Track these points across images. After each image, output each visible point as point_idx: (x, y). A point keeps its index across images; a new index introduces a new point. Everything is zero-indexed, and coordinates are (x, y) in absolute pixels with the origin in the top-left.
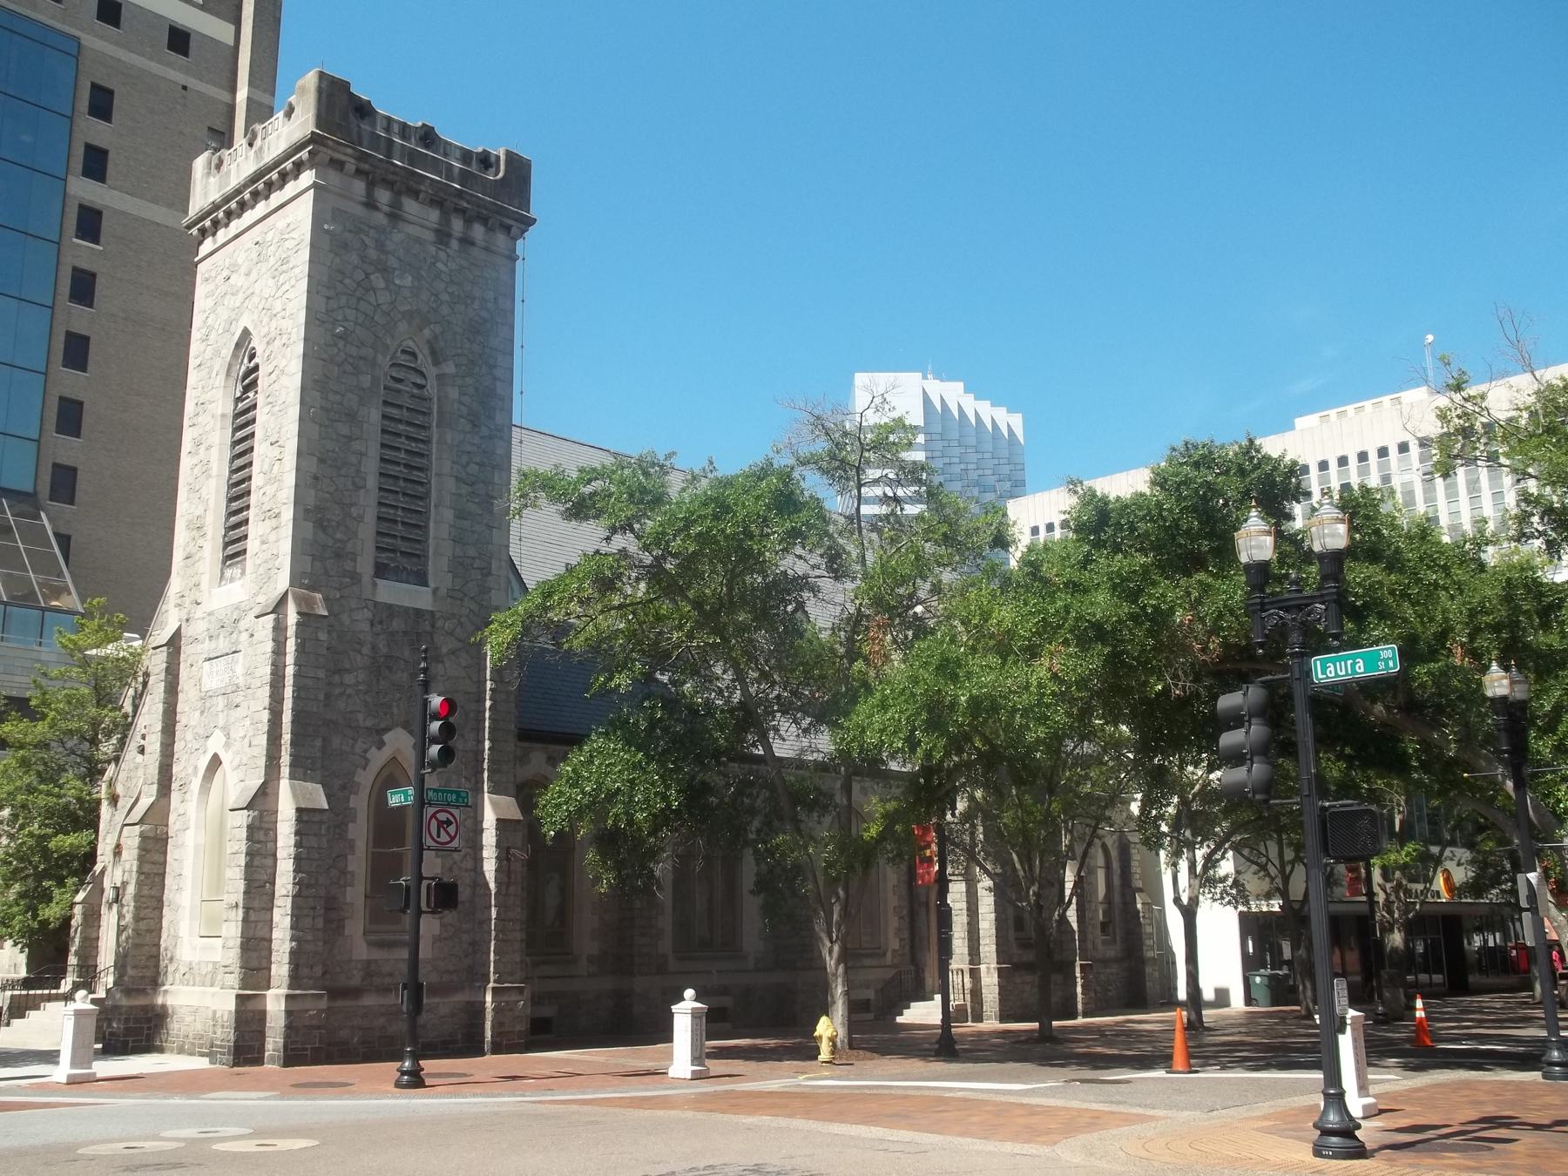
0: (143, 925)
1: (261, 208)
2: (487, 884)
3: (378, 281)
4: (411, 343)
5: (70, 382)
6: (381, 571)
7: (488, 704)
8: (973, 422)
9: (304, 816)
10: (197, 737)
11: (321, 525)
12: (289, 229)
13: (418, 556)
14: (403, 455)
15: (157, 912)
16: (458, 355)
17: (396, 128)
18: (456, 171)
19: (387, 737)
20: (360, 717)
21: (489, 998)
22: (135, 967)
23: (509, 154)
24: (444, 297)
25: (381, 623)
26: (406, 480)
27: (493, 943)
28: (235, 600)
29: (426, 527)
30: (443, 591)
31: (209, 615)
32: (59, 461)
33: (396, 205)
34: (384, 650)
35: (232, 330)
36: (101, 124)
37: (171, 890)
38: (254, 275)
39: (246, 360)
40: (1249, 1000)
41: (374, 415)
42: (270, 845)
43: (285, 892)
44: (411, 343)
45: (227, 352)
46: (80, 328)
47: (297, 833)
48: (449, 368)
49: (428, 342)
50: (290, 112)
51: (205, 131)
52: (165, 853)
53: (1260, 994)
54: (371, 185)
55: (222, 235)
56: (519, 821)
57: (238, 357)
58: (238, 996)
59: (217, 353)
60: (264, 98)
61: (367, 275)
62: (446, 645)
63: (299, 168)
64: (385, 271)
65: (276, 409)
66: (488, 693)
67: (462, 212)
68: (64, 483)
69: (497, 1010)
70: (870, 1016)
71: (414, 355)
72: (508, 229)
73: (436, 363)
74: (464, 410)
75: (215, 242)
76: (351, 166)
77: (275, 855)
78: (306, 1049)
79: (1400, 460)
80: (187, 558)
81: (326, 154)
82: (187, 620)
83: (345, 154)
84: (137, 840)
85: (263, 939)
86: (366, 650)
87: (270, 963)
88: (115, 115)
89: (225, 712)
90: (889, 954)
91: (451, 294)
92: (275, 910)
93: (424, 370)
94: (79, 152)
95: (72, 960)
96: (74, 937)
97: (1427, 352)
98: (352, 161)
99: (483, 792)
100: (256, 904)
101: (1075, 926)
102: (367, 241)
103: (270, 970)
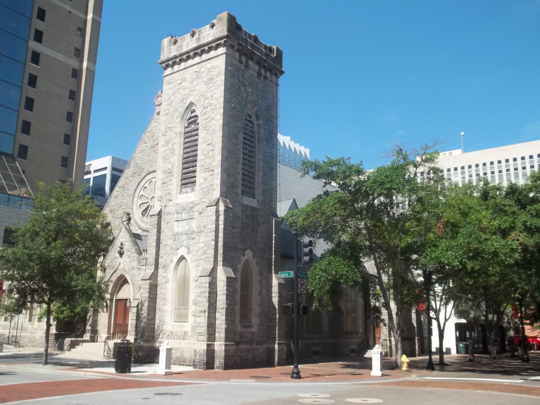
0: (150, 317)
1: (197, 59)
2: (274, 306)
3: (243, 89)
4: (250, 112)
5: (26, 115)
6: (243, 193)
7: (274, 242)
8: (288, 148)
9: (229, 280)
10: (171, 249)
11: (228, 175)
12: (213, 68)
13: (251, 188)
14: (248, 152)
15: (154, 312)
16: (263, 118)
17: (248, 36)
18: (264, 53)
19: (246, 252)
20: (239, 244)
21: (276, 346)
22: (148, 332)
23: (277, 48)
24: (260, 97)
25: (244, 211)
26: (249, 161)
27: (277, 327)
28: (190, 200)
29: (254, 178)
30: (260, 201)
31: (177, 205)
32: (22, 143)
33: (247, 62)
34: (245, 221)
35: (185, 101)
36: (41, 22)
37: (160, 304)
38: (195, 83)
39: (190, 113)
40: (458, 352)
41: (241, 136)
42: (215, 290)
43: (222, 307)
44: (250, 112)
45: (182, 110)
46: (31, 96)
47: (227, 286)
48: (261, 122)
49: (256, 112)
50: (213, 26)
51: (76, 28)
52: (156, 291)
53: (462, 350)
54: (240, 55)
55: (183, 65)
56: (284, 284)
57: (186, 112)
58: (207, 344)
59: (176, 110)
60: (97, 18)
61: (240, 87)
62: (261, 220)
63: (218, 46)
64: (245, 86)
65: (210, 132)
66: (274, 238)
67: (264, 67)
68: (23, 151)
69: (279, 351)
70: (355, 354)
71: (250, 116)
72: (276, 75)
73: (258, 119)
74: (265, 138)
75: (173, 70)
76: (236, 47)
77: (216, 293)
78: (230, 364)
79: (455, 173)
80: (163, 183)
81: (230, 42)
82: (165, 206)
83: (235, 43)
84: (148, 286)
85: (213, 324)
86: (240, 221)
87: (215, 332)
88: (46, 19)
89: (187, 241)
90: (360, 334)
91: (261, 96)
92: (217, 313)
93: (253, 122)
94: (33, 32)
95: (88, 328)
96: (89, 319)
97: (462, 138)
98: (237, 45)
99: (272, 273)
100: (211, 311)
101: (415, 325)
102: (240, 74)
103: (215, 335)
